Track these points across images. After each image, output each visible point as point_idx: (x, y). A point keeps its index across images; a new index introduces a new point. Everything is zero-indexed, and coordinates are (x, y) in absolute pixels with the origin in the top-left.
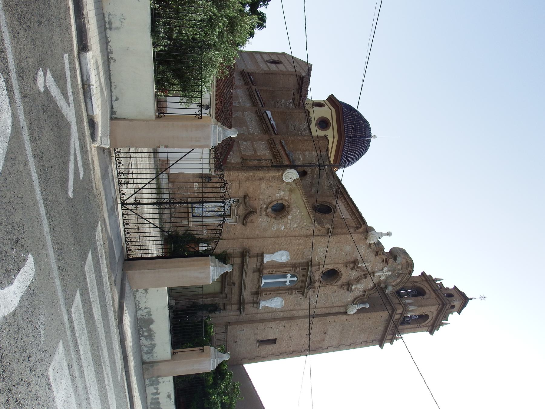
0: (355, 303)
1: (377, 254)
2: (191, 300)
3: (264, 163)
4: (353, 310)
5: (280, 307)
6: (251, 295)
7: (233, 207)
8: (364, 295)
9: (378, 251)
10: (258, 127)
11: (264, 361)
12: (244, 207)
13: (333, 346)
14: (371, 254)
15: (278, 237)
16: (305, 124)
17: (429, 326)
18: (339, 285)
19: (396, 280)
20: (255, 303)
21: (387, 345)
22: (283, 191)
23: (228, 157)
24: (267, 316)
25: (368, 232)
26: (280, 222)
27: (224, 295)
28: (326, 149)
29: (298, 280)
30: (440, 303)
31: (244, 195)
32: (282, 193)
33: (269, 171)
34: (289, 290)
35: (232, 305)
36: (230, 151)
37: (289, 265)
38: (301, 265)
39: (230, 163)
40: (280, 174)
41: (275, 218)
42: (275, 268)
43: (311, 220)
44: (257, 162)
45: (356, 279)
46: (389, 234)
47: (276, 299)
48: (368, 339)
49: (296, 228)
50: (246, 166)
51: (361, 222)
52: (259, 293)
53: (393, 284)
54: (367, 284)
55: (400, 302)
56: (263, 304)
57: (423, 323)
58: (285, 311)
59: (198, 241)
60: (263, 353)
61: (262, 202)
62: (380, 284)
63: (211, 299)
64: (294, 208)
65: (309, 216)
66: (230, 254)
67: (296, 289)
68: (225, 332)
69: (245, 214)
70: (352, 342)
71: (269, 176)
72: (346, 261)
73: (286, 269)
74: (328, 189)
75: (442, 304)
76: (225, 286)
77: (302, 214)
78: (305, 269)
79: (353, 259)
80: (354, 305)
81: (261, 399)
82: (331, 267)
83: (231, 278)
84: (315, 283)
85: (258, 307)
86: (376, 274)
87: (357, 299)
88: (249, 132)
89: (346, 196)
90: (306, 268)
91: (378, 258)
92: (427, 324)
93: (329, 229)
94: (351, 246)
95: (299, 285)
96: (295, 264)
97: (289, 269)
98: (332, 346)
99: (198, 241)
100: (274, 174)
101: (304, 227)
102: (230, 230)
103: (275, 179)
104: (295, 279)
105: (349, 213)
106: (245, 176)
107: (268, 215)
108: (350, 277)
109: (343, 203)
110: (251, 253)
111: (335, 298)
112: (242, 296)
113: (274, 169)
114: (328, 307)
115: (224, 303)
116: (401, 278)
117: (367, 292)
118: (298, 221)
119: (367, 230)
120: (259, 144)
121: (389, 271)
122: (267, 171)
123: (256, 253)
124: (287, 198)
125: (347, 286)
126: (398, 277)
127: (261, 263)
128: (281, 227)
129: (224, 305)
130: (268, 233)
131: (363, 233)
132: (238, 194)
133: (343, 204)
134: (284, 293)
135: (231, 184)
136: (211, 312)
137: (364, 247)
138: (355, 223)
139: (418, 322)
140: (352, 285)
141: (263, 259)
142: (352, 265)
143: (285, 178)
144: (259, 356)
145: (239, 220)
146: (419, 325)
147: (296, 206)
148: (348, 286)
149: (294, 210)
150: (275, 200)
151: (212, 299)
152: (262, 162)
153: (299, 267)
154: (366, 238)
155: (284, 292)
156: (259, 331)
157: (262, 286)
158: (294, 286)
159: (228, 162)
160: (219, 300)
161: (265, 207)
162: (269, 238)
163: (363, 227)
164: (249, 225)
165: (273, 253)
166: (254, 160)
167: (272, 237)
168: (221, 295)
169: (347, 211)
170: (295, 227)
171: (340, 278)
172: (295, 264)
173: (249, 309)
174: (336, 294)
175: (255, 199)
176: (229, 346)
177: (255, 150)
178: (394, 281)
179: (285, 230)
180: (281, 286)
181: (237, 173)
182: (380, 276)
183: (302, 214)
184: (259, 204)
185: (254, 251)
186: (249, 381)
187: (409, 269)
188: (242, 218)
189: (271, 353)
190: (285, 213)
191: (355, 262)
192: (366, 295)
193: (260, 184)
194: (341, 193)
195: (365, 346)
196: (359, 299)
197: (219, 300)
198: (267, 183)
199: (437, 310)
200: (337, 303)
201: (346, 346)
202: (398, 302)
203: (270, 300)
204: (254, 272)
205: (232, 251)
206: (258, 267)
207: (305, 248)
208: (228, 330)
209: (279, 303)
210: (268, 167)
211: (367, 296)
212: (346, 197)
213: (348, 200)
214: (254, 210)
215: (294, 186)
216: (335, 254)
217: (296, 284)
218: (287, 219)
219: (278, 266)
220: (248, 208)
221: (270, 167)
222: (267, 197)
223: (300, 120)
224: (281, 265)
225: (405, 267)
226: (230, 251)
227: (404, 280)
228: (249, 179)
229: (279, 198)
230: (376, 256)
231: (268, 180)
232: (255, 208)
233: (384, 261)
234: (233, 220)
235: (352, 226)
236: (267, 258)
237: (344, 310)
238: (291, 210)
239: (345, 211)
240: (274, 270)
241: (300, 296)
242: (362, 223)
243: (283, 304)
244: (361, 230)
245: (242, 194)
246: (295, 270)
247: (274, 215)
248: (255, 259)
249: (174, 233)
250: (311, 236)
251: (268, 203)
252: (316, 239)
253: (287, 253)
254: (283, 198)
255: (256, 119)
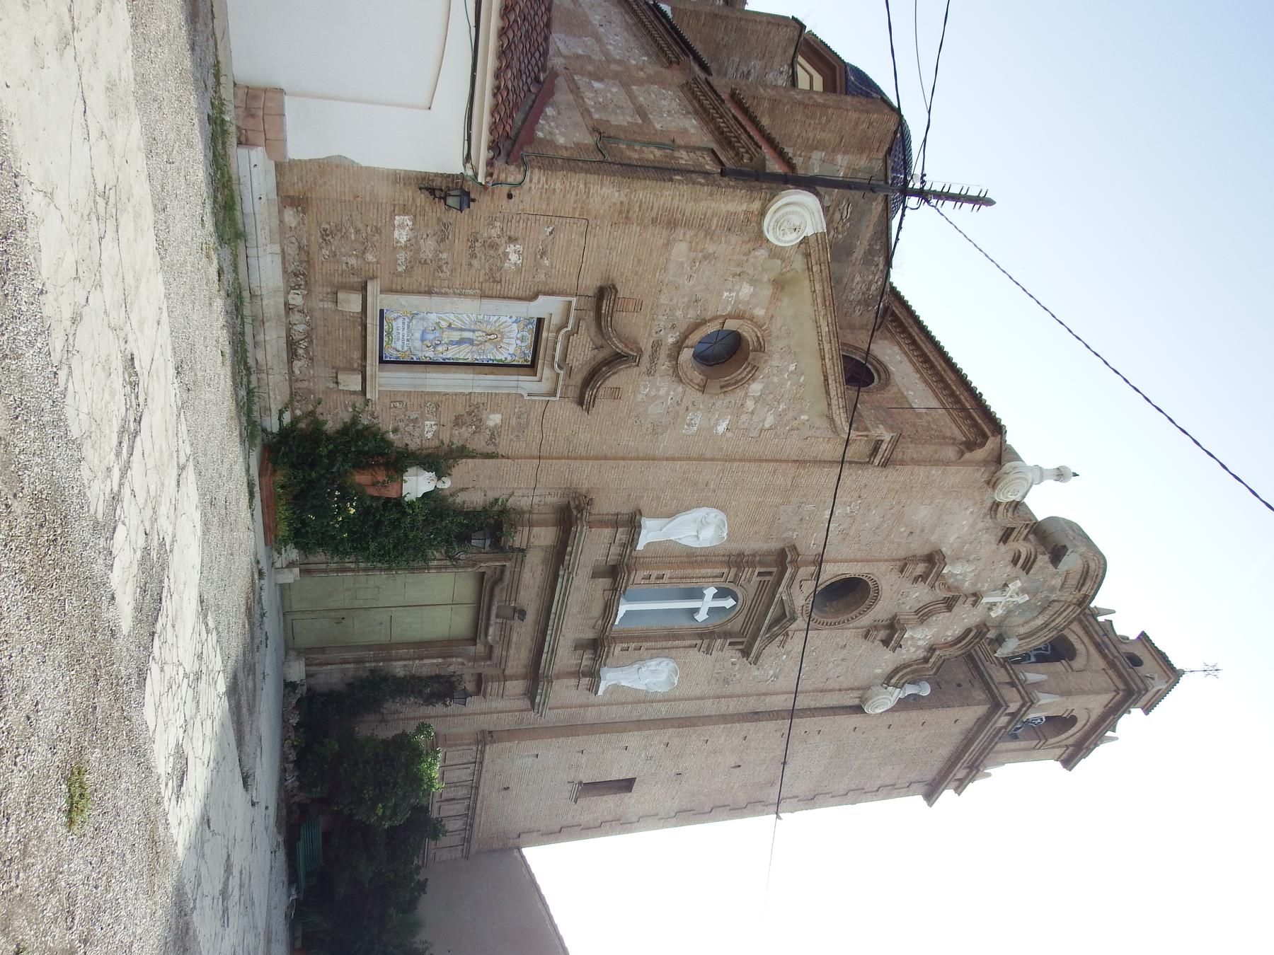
0: (893, 681)
1: (1007, 538)
2: (364, 662)
3: (684, 158)
4: (884, 700)
5: (663, 689)
6: (576, 648)
7: (548, 330)
8: (926, 660)
9: (1013, 529)
10: (637, 42)
11: (587, 837)
12: (593, 334)
13: (797, 797)
14: (986, 536)
15: (702, 458)
16: (781, 73)
17: (1067, 747)
18: (862, 628)
19: (1034, 619)
20: (584, 675)
21: (948, 795)
22: (754, 282)
23: (537, 122)
24: (616, 713)
25: (1000, 463)
26: (719, 403)
27: (480, 648)
28: (885, 149)
29: (738, 608)
30: (1121, 686)
31: (599, 285)
32: (746, 290)
33: (715, 188)
34: (701, 636)
35: (505, 680)
36: (544, 104)
37: (720, 558)
38: (758, 558)
39: (551, 143)
40: (756, 206)
41: (703, 388)
42: (670, 565)
43: (829, 405)
44: (658, 153)
45: (917, 612)
46: (1061, 474)
47: (653, 663)
48: (898, 778)
49: (771, 428)
50: (618, 160)
51: (984, 426)
52: (602, 645)
53: (1022, 630)
54: (949, 626)
55: (1011, 677)
56: (611, 677)
57: (1055, 736)
58: (675, 700)
59: (399, 461)
60: (585, 818)
61: (662, 321)
62: (985, 630)
63: (435, 661)
64: (776, 356)
65: (823, 390)
66: (521, 512)
67: (726, 635)
68: (475, 763)
69: (593, 363)
70: (853, 787)
71: (709, 212)
72: (902, 553)
73: (709, 570)
74: (859, 303)
75: (1124, 690)
76: (488, 619)
77: (801, 380)
78: (770, 573)
79: (926, 550)
80: (890, 689)
81: (562, 931)
82: (852, 570)
83: (513, 594)
84: (793, 619)
85: (593, 688)
86: (985, 600)
87: (905, 671)
88: (607, 54)
89: (914, 331)
90: (774, 570)
91: (1003, 548)
92: (1066, 739)
93: (878, 444)
94: (934, 505)
95: (737, 625)
96: (741, 555)
97: (717, 571)
98: (794, 797)
99: (399, 461)
100: (731, 207)
101: (798, 429)
102: (528, 424)
103: (729, 225)
104: (729, 603)
105: (933, 391)
106: (615, 204)
107: (678, 376)
108: (903, 603)
109: (905, 353)
110: (593, 512)
111: (838, 665)
112: (544, 656)
113: (731, 183)
114: (809, 692)
115: (480, 675)
116: (1052, 613)
117: (937, 653)
118: (782, 407)
119: (1000, 455)
120: (654, 96)
121: (1023, 591)
122: (706, 188)
123: (614, 510)
124: (759, 312)
125: (887, 632)
126: (1044, 609)
127: (624, 546)
128: (716, 424)
129: (480, 680)
130: (666, 443)
131: (985, 465)
132: (574, 280)
133: (906, 359)
134: (685, 647)
135: (551, 233)
136: (430, 700)
137: (972, 513)
138: (959, 427)
139: (1040, 734)
140: (904, 630)
141: (636, 536)
142: (921, 568)
143: (771, 228)
144: (575, 824)
145: (566, 386)
146: (1042, 742)
147: (789, 346)
148: (891, 631)
149: (775, 363)
150: (715, 318)
151: (440, 660)
152: (676, 154)
153: (752, 565)
154: (992, 483)
155: (688, 643)
156: (584, 759)
157: (617, 623)
158: (721, 625)
159: (541, 140)
160: (463, 664)
161: (671, 340)
162: (667, 459)
163: (991, 443)
164: (603, 406)
165: (671, 515)
166: (648, 144)
167: (679, 459)
168: (471, 649)
169: (925, 381)
170: (767, 425)
171: (870, 607)
172: (739, 555)
173: (564, 693)
174: (843, 653)
175: (639, 306)
176: (482, 802)
177: (640, 111)
178: (1027, 622)
179: (729, 435)
180: (685, 623)
181: (582, 186)
182: (991, 606)
183: (801, 380)
184: (651, 329)
185: (607, 505)
186: (540, 906)
187: (1085, 589)
188: (578, 379)
189: (609, 818)
190: (740, 373)
191: (933, 560)
192: (932, 660)
193: (668, 244)
194: (896, 319)
195: (887, 797)
196: (909, 669)
197: (463, 664)
198: (697, 243)
199: (1106, 706)
200: (841, 679)
201: (832, 797)
202: (1008, 680)
203: (636, 666)
204: (595, 575)
205: (524, 503)
206: (613, 558)
207: (783, 504)
208: (487, 756)
209: (663, 677)
210: (706, 174)
211: (934, 663)
212: (914, 334)
213: (923, 346)
214: (632, 350)
215: (799, 263)
216: (878, 528)
217: (730, 620)
218: (746, 393)
219: (682, 559)
220: (610, 339)
221: (717, 177)
222: (686, 300)
223: (767, 55)
224: (694, 558)
225: (1074, 582)
226: (521, 501)
227: (1057, 621)
228: (627, 218)
229: (729, 308)
230: (1001, 543)
231: (703, 227)
232: (635, 342)
233: (1021, 561)
234: (545, 386)
235: (951, 438)
236: (652, 533)
237: (857, 702)
238: (766, 361)
239: (918, 381)
240: (668, 573)
241: (732, 657)
242: (986, 430)
243: (676, 682)
244: (980, 454)
245: (590, 283)
246: (736, 575)
247: (698, 377)
248: (607, 532)
249: (302, 425)
250: (850, 462)
251: (685, 327)
252: (851, 477)
253: (722, 516)
254: (744, 312)
255: (627, 23)
